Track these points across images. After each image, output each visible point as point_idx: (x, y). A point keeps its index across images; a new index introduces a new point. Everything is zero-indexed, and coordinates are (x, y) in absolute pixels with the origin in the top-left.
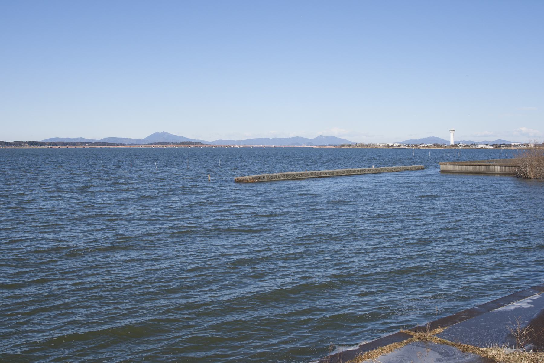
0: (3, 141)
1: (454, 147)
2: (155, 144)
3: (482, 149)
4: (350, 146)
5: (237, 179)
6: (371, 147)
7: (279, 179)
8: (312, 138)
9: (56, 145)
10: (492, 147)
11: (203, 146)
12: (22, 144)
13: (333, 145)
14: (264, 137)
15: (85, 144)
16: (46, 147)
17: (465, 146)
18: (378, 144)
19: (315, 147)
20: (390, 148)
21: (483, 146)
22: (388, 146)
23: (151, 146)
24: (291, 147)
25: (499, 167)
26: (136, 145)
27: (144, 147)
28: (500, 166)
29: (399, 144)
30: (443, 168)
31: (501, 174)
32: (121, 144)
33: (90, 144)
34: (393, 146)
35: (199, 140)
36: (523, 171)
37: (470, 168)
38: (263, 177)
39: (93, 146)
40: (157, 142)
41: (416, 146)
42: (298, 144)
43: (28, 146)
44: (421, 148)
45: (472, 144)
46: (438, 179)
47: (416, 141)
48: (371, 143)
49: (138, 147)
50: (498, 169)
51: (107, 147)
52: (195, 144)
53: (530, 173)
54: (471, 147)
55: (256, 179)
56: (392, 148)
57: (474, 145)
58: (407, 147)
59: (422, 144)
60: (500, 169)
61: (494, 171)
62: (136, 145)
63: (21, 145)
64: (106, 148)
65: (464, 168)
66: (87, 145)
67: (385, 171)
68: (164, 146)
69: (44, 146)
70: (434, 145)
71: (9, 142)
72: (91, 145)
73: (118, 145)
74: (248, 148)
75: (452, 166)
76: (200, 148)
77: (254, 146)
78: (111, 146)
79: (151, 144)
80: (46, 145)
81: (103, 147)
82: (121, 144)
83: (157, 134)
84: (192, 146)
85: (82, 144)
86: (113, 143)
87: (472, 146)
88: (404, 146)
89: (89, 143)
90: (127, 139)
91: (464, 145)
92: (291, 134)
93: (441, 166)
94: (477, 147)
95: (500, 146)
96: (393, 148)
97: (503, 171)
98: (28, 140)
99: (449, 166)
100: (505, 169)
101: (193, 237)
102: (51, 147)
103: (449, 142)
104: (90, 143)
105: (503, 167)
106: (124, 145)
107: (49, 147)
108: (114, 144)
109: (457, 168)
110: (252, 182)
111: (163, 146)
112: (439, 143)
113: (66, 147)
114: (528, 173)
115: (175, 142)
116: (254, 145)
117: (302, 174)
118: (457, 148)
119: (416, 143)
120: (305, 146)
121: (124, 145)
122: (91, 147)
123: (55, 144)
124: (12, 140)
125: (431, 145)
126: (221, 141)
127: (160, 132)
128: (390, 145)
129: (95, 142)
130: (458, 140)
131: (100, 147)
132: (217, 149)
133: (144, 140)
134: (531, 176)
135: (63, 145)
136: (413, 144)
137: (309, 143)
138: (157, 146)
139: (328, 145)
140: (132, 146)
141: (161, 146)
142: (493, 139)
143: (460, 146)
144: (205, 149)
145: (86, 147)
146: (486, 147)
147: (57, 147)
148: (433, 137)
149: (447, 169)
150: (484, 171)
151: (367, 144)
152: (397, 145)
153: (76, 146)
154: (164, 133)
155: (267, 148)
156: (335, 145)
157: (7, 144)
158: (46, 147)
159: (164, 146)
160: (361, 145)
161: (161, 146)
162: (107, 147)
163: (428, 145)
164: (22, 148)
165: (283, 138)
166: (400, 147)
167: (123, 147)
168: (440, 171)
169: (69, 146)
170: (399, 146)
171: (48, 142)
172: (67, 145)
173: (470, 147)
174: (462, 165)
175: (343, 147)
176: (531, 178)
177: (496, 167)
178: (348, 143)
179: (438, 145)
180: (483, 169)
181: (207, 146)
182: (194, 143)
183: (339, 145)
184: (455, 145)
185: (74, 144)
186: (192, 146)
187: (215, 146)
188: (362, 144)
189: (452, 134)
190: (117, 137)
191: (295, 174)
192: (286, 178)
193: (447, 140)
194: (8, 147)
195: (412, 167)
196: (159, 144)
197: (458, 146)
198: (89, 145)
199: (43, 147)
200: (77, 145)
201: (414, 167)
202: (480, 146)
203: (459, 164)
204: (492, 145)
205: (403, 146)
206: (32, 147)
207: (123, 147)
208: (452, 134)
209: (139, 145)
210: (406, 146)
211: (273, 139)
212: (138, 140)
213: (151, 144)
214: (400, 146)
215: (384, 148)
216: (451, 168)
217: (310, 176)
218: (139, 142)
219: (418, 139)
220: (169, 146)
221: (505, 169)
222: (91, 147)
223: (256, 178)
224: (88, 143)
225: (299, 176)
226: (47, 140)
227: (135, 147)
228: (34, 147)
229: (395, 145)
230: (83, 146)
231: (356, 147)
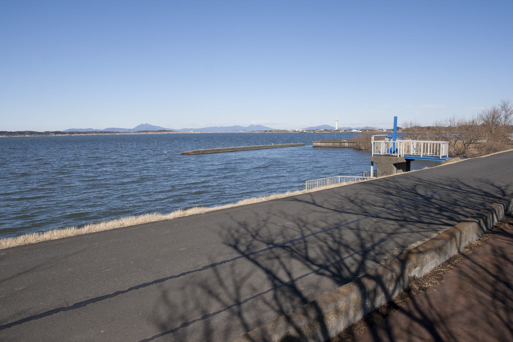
0: (36, 132)
1: (338, 132)
2: (141, 132)
3: (355, 133)
4: (271, 131)
5: (183, 153)
6: (285, 132)
7: (209, 152)
8: (246, 126)
9: (73, 134)
10: (361, 131)
11: (173, 133)
12: (50, 134)
13: (260, 131)
14: (214, 126)
15: (93, 132)
16: (66, 135)
17: (344, 131)
18: (289, 130)
19: (247, 132)
20: (296, 132)
21: (356, 131)
22: (295, 131)
23: (138, 134)
24: (232, 132)
25: (347, 143)
26: (128, 132)
27: (133, 134)
28: (348, 143)
29: (303, 130)
30: (315, 144)
31: (349, 147)
32: (118, 132)
33: (96, 133)
34: (298, 131)
35: (170, 129)
36: (358, 146)
37: (331, 144)
38: (199, 152)
39: (99, 134)
40: (142, 130)
41: (313, 131)
42: (237, 130)
43: (54, 135)
44: (317, 132)
45: (349, 130)
46: (312, 152)
47: (314, 127)
48: (284, 129)
49: (129, 134)
50: (346, 144)
51: (108, 134)
52: (168, 132)
53: (362, 147)
54: (348, 132)
55: (194, 153)
56: (298, 132)
57: (351, 130)
58: (307, 132)
59: (317, 130)
60: (348, 144)
61: (345, 146)
62: (128, 132)
63: (49, 134)
64: (107, 135)
65: (327, 144)
66: (94, 133)
67: (279, 147)
68: (147, 133)
69: (65, 134)
70: (325, 130)
71: (41, 132)
72: (97, 133)
73: (115, 133)
74: (203, 133)
75: (320, 143)
76: (170, 135)
77: (208, 132)
78: (111, 134)
79: (138, 132)
80: (66, 133)
81: (105, 134)
82: (118, 132)
83: (142, 125)
84: (166, 133)
85: (91, 132)
86: (112, 131)
87: (349, 131)
88: (306, 131)
89: (96, 132)
90: (121, 128)
91: (343, 130)
92: (255, 122)
93: (314, 143)
94: (352, 132)
95: (366, 130)
96: (299, 133)
97: (350, 145)
98: (54, 131)
99: (318, 143)
100: (351, 144)
101: (47, 168)
102: (70, 135)
103: (335, 128)
104: (96, 132)
105: (350, 143)
106: (119, 133)
107: (68, 135)
108: (113, 132)
109: (323, 144)
110: (192, 155)
111: (146, 133)
112: (329, 129)
113: (80, 135)
114: (361, 147)
115: (154, 130)
116: (208, 131)
117: (224, 149)
118: (339, 132)
119: (314, 129)
120: (241, 132)
121: (119, 133)
122: (97, 134)
123: (73, 133)
124: (42, 131)
125: (323, 130)
126: (185, 129)
127: (144, 123)
128: (297, 130)
129: (100, 131)
130: (341, 127)
131: (103, 134)
132: (182, 134)
133: (133, 129)
134: (363, 148)
135: (78, 134)
136: (311, 129)
137: (244, 130)
138: (142, 133)
139: (256, 131)
140: (125, 134)
141: (144, 133)
142: (363, 126)
143: (341, 130)
144: (174, 134)
145: (93, 134)
146: (357, 131)
147: (74, 135)
148: (325, 125)
149: (317, 145)
150: (339, 146)
151: (282, 130)
152: (301, 130)
153: (87, 134)
154: (147, 124)
155: (216, 133)
156: (261, 131)
157: (39, 133)
158: (66, 135)
159: (147, 133)
160: (278, 131)
161: (144, 133)
162: (108, 134)
163: (321, 130)
164: (50, 136)
165: (227, 127)
166: (303, 132)
167: (119, 134)
168: (313, 146)
169: (82, 134)
170: (302, 131)
171: (67, 131)
172: (80, 133)
173: (347, 131)
174: (326, 143)
175: (266, 132)
176: (363, 150)
177: (346, 143)
178: (270, 130)
179: (327, 131)
180: (338, 144)
181: (176, 133)
182: (166, 131)
183: (263, 131)
184: (338, 130)
185: (85, 133)
186: (166, 133)
187: (181, 132)
188: (278, 130)
189: (337, 123)
190: (115, 127)
191: (220, 149)
192: (213, 152)
193: (334, 127)
194: (40, 136)
195: (297, 144)
196: (143, 132)
197: (340, 131)
198: (95, 133)
199: (64, 135)
200: (87, 134)
201: (298, 144)
202: (353, 131)
203: (324, 141)
204: (361, 130)
205: (305, 131)
206: (57, 135)
207: (119, 134)
208: (337, 123)
209: (130, 132)
210: (307, 131)
211: (220, 128)
212: (129, 130)
213: (138, 132)
214: (303, 131)
215: (293, 132)
216: (319, 144)
217: (230, 151)
218: (129, 131)
219: (316, 126)
220: (150, 133)
221: (351, 144)
222: (97, 134)
223: (194, 152)
224: (95, 132)
225: (222, 150)
226: (66, 130)
227: (127, 134)
228: (58, 135)
229: (300, 131)
230: (92, 134)
231: (274, 132)
